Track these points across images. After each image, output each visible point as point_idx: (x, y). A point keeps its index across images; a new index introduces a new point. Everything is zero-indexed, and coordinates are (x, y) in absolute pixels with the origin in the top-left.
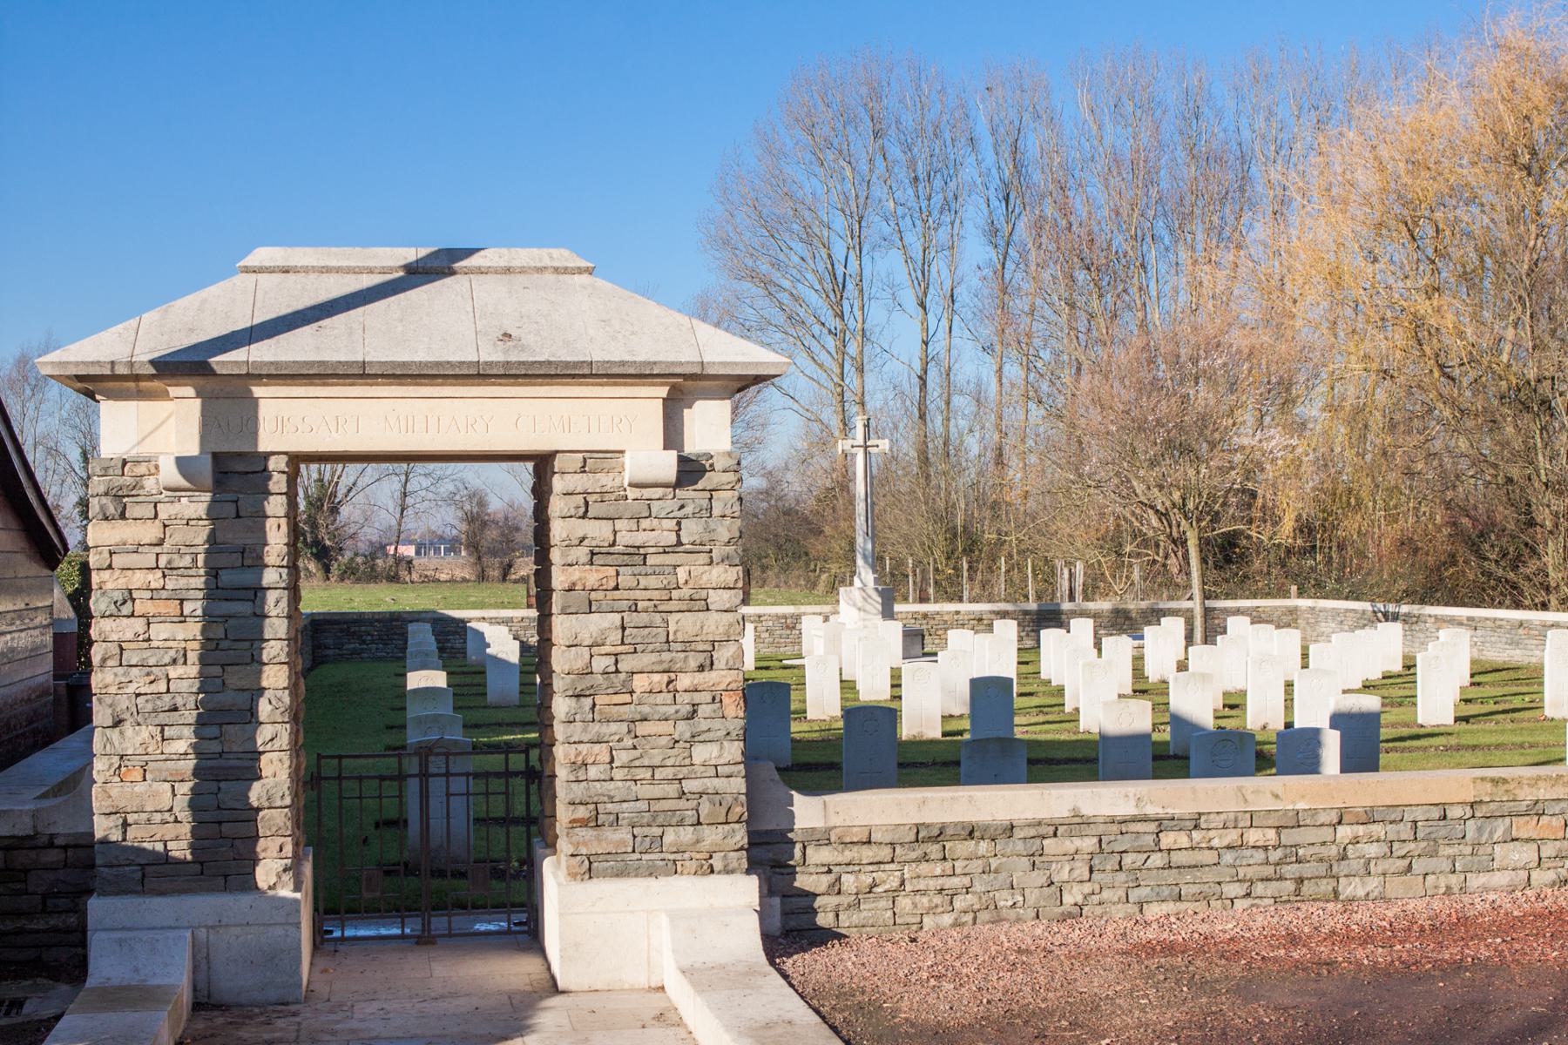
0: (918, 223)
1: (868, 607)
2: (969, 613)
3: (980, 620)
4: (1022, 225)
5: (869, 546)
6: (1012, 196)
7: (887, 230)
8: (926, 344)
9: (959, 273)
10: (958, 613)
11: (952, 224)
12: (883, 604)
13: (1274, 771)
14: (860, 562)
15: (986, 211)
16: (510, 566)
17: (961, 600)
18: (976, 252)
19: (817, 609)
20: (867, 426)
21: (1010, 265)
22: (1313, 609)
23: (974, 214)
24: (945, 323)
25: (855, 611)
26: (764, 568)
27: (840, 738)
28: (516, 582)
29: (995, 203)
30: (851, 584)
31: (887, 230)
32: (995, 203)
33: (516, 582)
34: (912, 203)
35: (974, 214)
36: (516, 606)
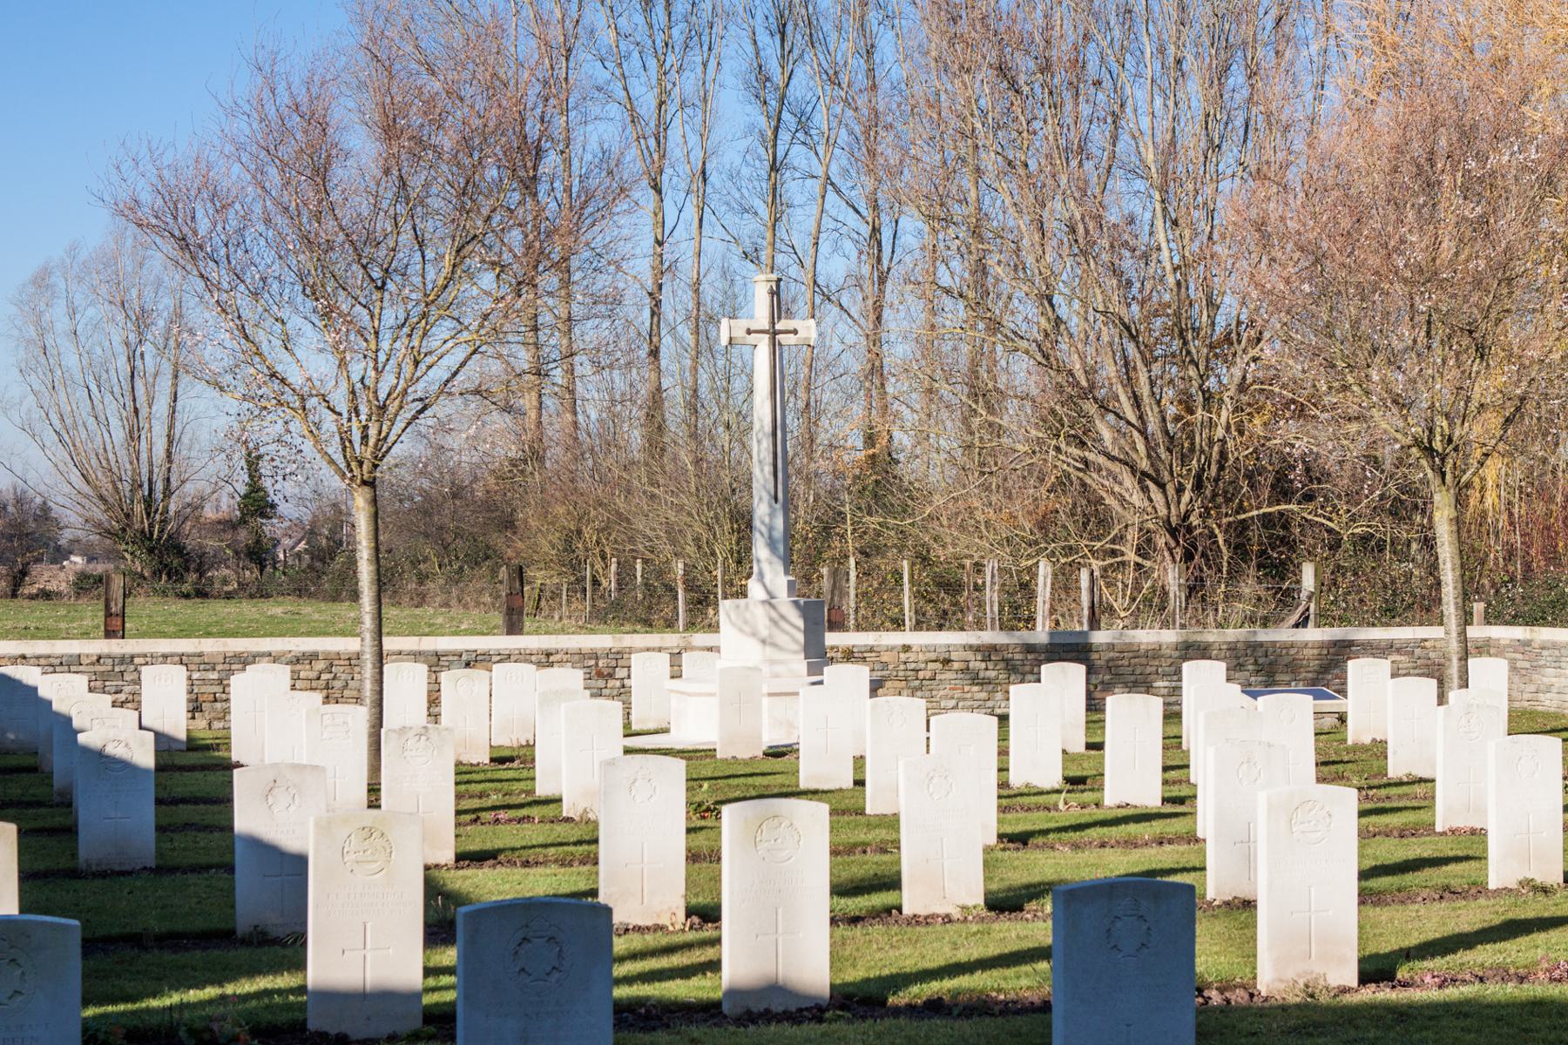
0: (652, 63)
1: (782, 639)
2: (926, 649)
3: (947, 662)
4: (802, 75)
5: (779, 522)
6: (790, 27)
7: (602, 75)
8: (660, 243)
9: (715, 138)
10: (907, 648)
11: (705, 65)
12: (806, 632)
13: (1063, 888)
14: (761, 550)
15: (750, 49)
16: (24, 573)
17: (898, 624)
18: (736, 113)
19: (654, 639)
20: (775, 293)
21: (784, 136)
22: (1528, 643)
23: (734, 54)
24: (691, 213)
25: (754, 645)
26: (422, 578)
27: (1050, 947)
28: (32, 597)
29: (764, 38)
30: (742, 593)
31: (602, 75)
32: (764, 38)
33: (32, 597)
34: (641, 34)
35: (734, 54)
36: (85, 635)
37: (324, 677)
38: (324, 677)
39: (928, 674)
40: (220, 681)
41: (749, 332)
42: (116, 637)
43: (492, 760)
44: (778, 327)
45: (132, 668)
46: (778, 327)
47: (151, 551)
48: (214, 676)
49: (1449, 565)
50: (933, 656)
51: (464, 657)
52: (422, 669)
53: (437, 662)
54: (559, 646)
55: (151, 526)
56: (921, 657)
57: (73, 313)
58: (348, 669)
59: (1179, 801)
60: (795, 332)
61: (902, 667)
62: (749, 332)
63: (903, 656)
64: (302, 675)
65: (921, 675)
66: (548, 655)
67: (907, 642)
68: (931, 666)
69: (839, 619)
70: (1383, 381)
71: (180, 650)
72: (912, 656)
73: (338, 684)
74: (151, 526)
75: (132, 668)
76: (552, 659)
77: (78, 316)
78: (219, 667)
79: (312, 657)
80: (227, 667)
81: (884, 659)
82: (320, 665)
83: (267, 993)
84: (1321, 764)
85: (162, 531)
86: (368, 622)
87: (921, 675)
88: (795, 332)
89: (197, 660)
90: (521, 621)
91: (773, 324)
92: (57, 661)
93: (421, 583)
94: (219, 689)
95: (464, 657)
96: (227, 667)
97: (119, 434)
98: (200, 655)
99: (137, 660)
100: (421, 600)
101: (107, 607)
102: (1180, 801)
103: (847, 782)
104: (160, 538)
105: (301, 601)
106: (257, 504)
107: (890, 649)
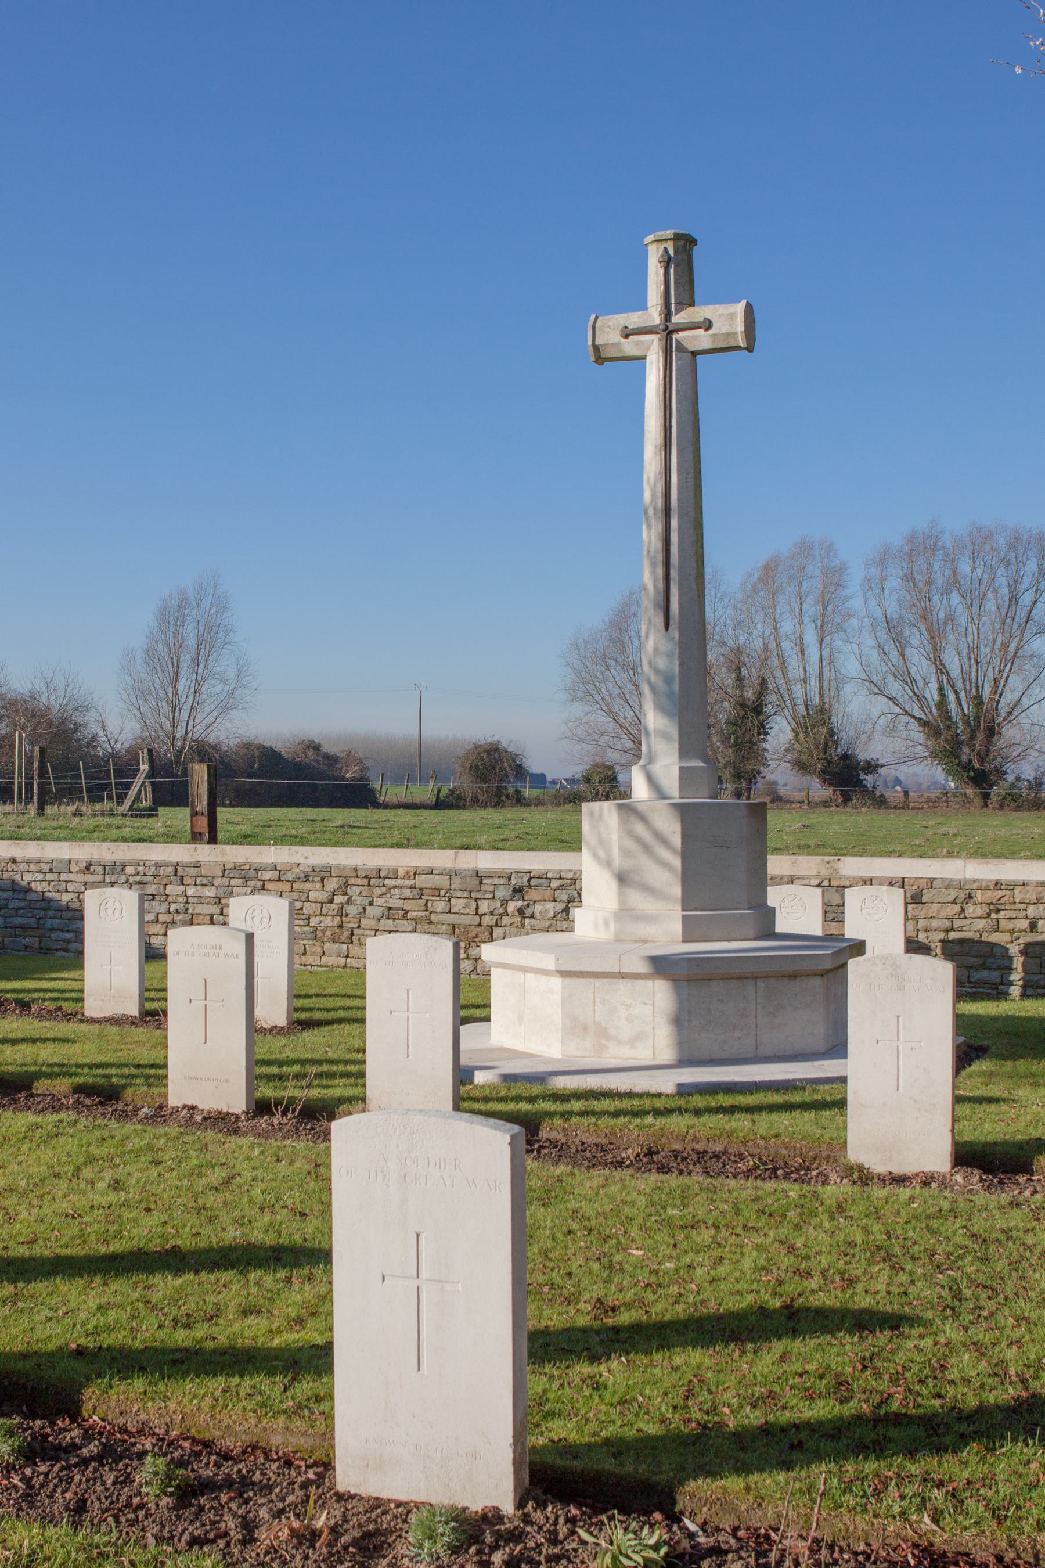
37: (339, 899)
38: (339, 899)
40: (218, 900)
43: (967, 1156)
46: (675, 319)
48: (209, 892)
58: (365, 891)
59: (153, 1015)
60: (708, 325)
64: (313, 895)
70: (197, 1519)
73: (352, 910)
79: (323, 873)
80: (226, 881)
82: (332, 884)
83: (980, 853)
84: (841, 1104)
88: (708, 325)
89: (193, 871)
91: (667, 315)
92: (46, 868)
94: (216, 910)
98: (197, 865)
99: (130, 870)
102: (153, 1013)
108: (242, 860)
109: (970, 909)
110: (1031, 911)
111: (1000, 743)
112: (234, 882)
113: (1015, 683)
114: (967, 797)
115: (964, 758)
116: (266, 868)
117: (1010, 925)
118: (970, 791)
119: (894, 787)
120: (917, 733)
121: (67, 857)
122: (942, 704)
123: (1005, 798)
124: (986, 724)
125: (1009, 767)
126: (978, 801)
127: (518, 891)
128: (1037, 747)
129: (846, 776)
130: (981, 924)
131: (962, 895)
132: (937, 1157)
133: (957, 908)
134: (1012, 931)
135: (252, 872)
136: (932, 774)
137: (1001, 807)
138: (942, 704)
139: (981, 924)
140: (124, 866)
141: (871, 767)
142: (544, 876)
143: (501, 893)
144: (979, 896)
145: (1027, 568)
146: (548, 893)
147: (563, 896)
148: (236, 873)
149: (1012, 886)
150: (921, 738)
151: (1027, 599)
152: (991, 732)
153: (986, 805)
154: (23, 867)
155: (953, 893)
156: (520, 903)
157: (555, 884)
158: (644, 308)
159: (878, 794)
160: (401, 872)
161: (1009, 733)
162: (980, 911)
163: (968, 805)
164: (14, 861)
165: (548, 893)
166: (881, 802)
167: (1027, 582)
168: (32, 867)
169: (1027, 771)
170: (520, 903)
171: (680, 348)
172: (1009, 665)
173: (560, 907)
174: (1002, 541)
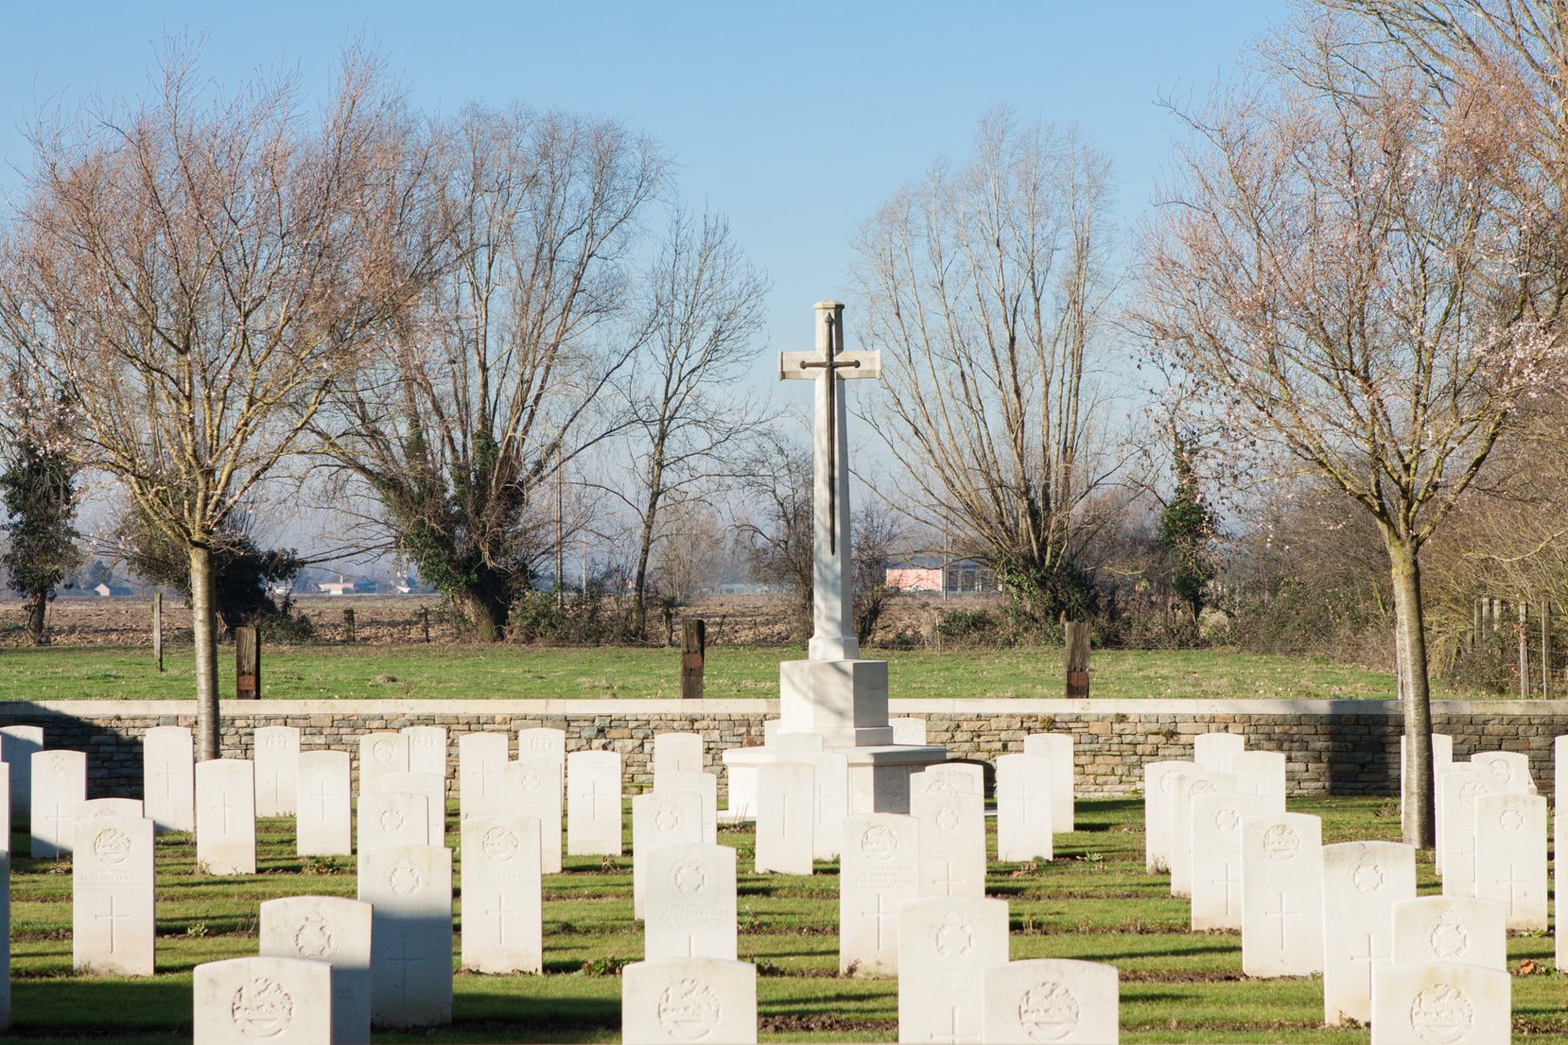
10: (1122, 718)
39: (1148, 749)
41: (804, 365)
42: (248, 697)
44: (836, 359)
45: (233, 730)
46: (836, 359)
47: (1042, 583)
49: (1406, 628)
50: (1154, 727)
51: (597, 723)
52: (440, 732)
53: (454, 728)
54: (705, 711)
55: (1042, 550)
56: (1140, 728)
57: (938, 257)
60: (857, 364)
61: (1116, 740)
62: (804, 365)
63: (1117, 727)
65: (1140, 749)
66: (693, 721)
67: (1122, 711)
68: (1152, 739)
69: (1081, 683)
71: (284, 712)
72: (1128, 728)
74: (1042, 550)
75: (233, 730)
76: (696, 725)
77: (946, 262)
78: (326, 731)
80: (335, 730)
81: (1094, 730)
85: (1055, 556)
86: (203, 684)
87: (1140, 749)
88: (857, 364)
90: (699, 683)
91: (831, 356)
93: (1356, 631)
95: (597, 723)
96: (335, 730)
97: (996, 422)
98: (306, 718)
99: (238, 723)
100: (1269, 651)
101: (239, 665)
103: (617, 850)
104: (1053, 565)
105: (1246, 656)
106: (1189, 519)
107: (1100, 719)
108: (351, 712)
109: (959, 736)
110: (1003, 736)
111: (525, 519)
112: (342, 731)
113: (554, 408)
114: (465, 621)
115: (461, 549)
116: (373, 718)
117: (988, 746)
118: (470, 609)
119: (93, 586)
120: (368, 501)
121: (175, 713)
122: (417, 447)
123: (536, 622)
124: (497, 482)
125: (544, 566)
126: (486, 627)
127: (601, 731)
128: (594, 525)
129: (246, 589)
130: (967, 746)
131: (953, 725)
132: (1071, 829)
133: (949, 735)
134: (989, 751)
135: (360, 722)
136: (403, 582)
137: (529, 639)
138: (417, 447)
139: (967, 746)
140: (233, 720)
141: (285, 566)
142: (624, 720)
143: (585, 734)
144: (965, 726)
145: (571, 190)
146: (626, 732)
147: (641, 734)
148: (345, 723)
149: (988, 718)
150: (377, 508)
151: (572, 249)
152: (514, 497)
153: (501, 636)
154: (127, 723)
155: (946, 724)
156: (603, 741)
157: (634, 724)
158: (813, 348)
159: (294, 614)
160: (498, 719)
161: (539, 499)
162: (966, 736)
163: (466, 636)
164: (119, 718)
165: (626, 732)
166: (303, 631)
167: (570, 217)
168: (138, 723)
169: (577, 569)
170: (603, 741)
171: (840, 377)
172: (540, 371)
173: (638, 742)
174: (527, 143)
